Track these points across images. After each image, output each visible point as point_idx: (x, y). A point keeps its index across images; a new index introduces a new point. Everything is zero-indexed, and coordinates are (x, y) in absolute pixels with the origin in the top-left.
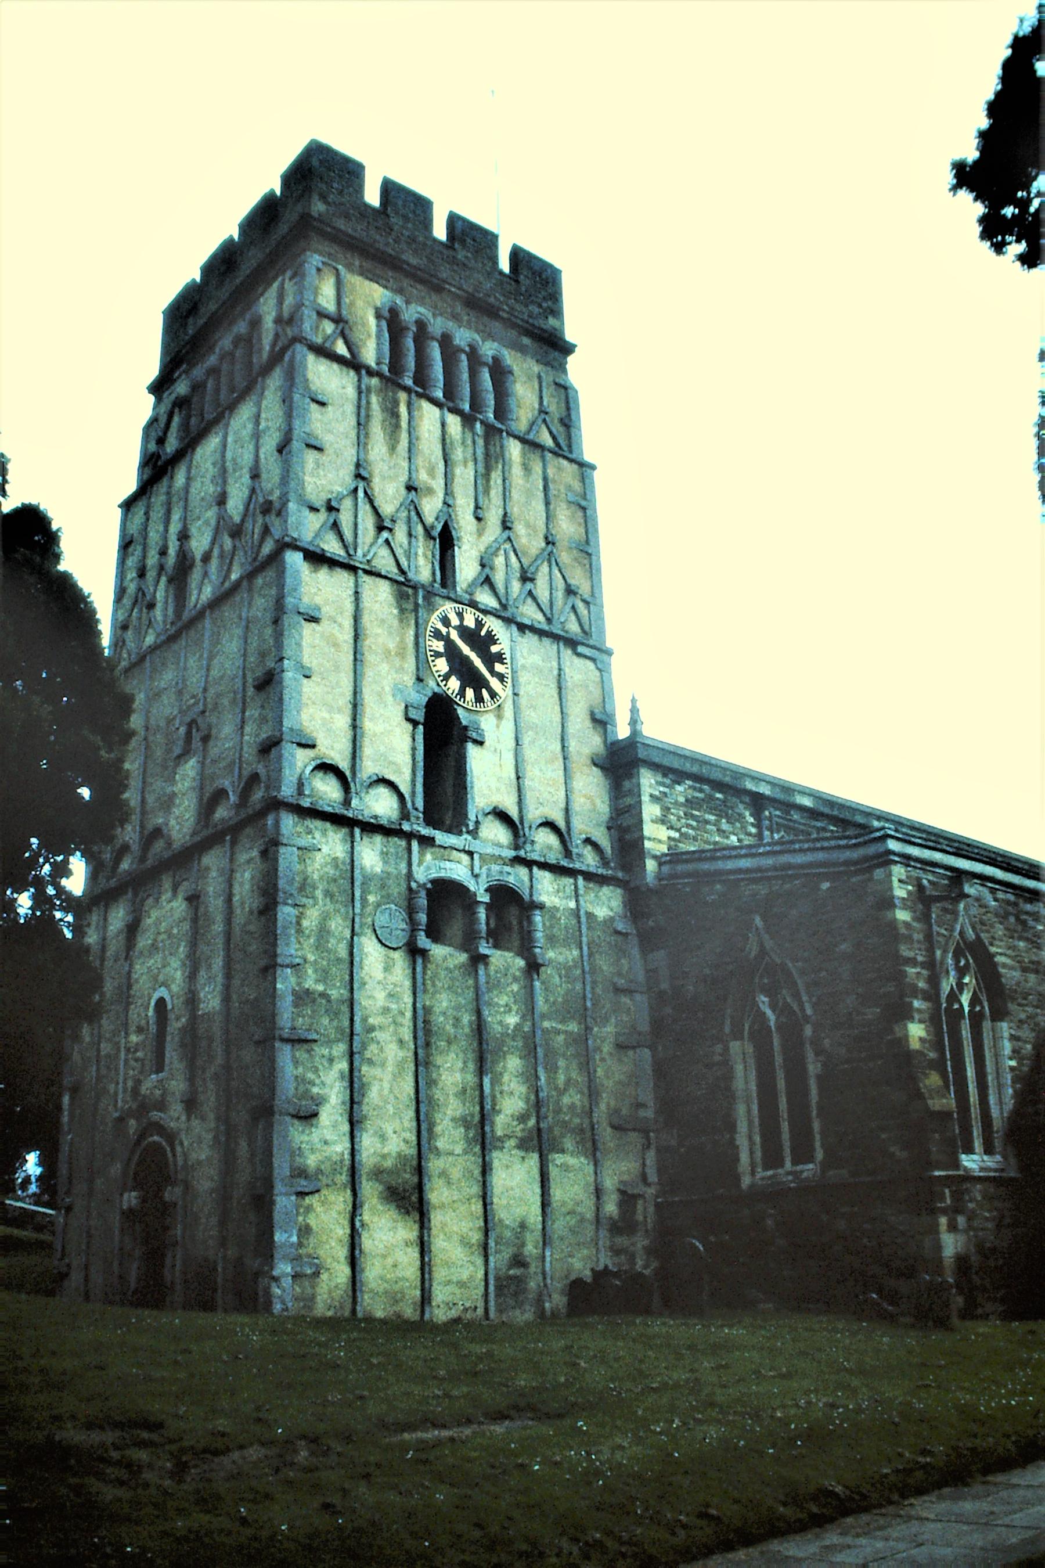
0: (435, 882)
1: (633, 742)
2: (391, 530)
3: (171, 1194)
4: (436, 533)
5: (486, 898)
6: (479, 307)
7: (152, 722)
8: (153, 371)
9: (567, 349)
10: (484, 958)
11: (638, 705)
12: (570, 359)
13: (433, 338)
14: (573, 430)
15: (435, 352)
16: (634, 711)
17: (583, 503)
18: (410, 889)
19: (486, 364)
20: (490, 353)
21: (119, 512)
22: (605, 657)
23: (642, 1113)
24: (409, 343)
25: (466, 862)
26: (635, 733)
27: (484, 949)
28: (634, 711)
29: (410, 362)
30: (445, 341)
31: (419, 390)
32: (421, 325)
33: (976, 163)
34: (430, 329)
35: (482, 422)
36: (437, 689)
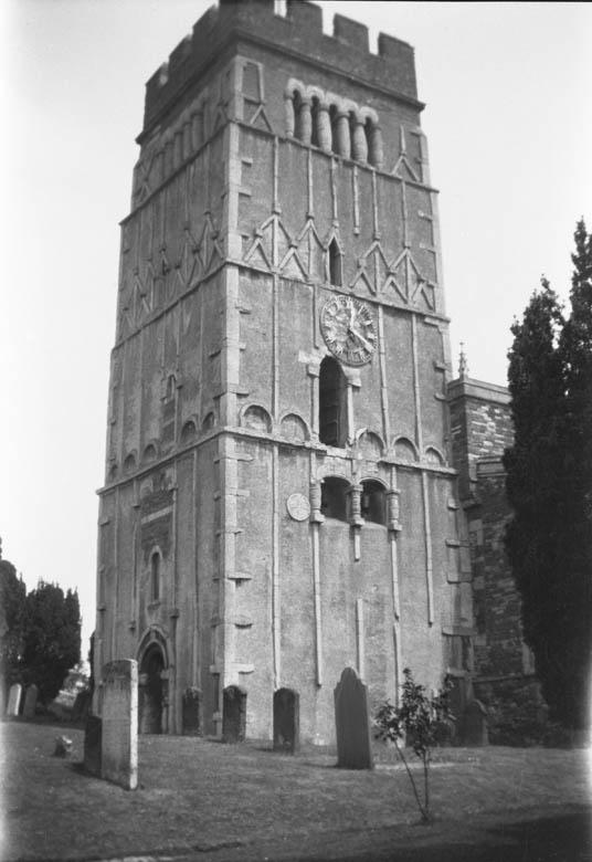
0: (326, 479)
1: (459, 385)
2: (296, 247)
3: (166, 674)
4: (326, 247)
5: (361, 489)
6: (354, 86)
7: (150, 568)
8: (139, 128)
9: (421, 107)
10: (359, 526)
11: (466, 357)
12: (423, 115)
13: (324, 109)
14: (424, 166)
15: (325, 119)
16: (462, 361)
17: (430, 217)
18: (310, 484)
19: (361, 124)
20: (365, 115)
21: (119, 228)
22: (443, 324)
23: (466, 625)
24: (307, 115)
25: (353, 464)
26: (462, 376)
27: (360, 521)
28: (462, 361)
29: (308, 129)
30: (333, 110)
31: (315, 148)
32: (315, 100)
33: (159, 677)
34: (321, 102)
35: (359, 166)
36: (329, 354)
